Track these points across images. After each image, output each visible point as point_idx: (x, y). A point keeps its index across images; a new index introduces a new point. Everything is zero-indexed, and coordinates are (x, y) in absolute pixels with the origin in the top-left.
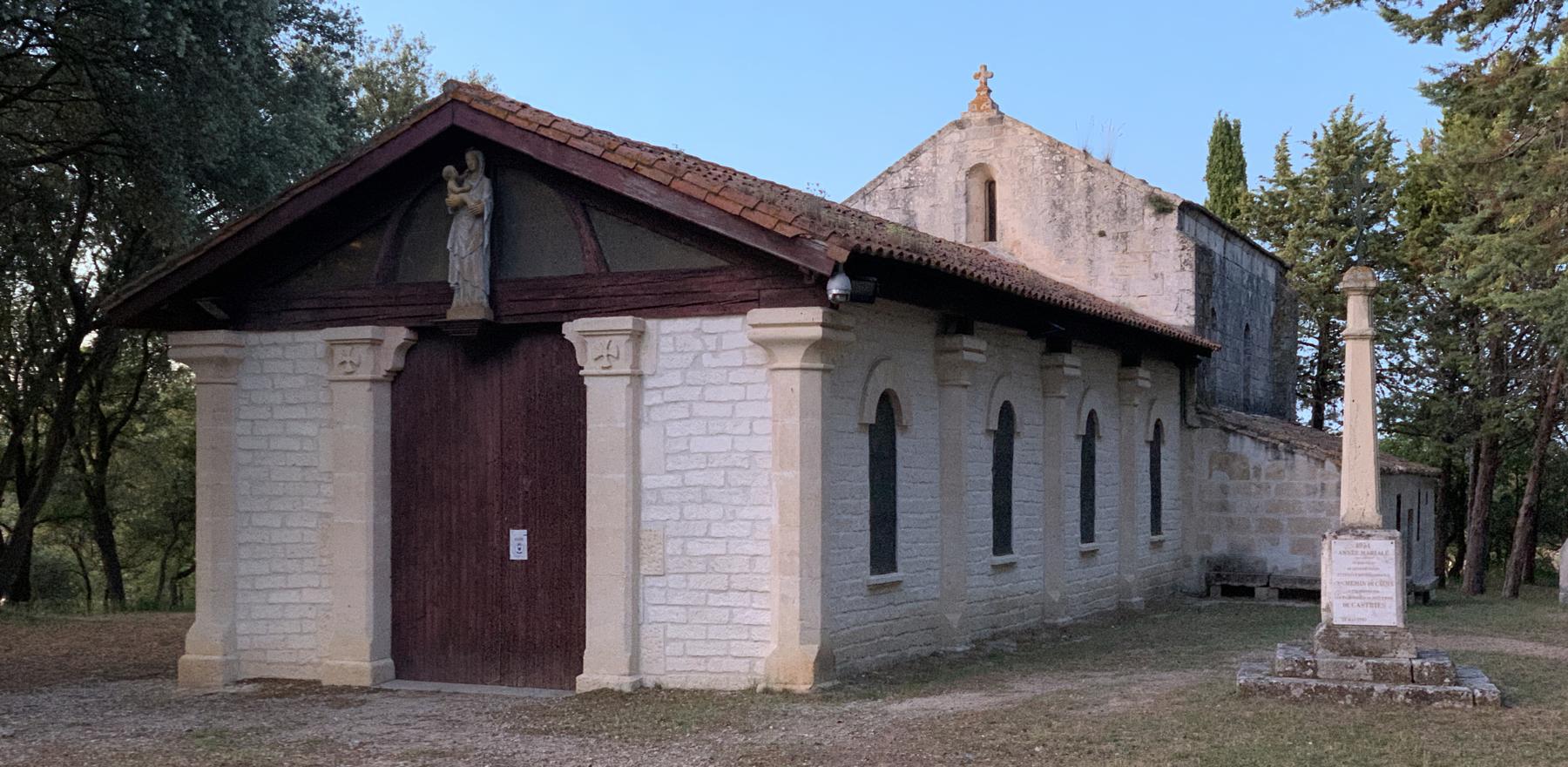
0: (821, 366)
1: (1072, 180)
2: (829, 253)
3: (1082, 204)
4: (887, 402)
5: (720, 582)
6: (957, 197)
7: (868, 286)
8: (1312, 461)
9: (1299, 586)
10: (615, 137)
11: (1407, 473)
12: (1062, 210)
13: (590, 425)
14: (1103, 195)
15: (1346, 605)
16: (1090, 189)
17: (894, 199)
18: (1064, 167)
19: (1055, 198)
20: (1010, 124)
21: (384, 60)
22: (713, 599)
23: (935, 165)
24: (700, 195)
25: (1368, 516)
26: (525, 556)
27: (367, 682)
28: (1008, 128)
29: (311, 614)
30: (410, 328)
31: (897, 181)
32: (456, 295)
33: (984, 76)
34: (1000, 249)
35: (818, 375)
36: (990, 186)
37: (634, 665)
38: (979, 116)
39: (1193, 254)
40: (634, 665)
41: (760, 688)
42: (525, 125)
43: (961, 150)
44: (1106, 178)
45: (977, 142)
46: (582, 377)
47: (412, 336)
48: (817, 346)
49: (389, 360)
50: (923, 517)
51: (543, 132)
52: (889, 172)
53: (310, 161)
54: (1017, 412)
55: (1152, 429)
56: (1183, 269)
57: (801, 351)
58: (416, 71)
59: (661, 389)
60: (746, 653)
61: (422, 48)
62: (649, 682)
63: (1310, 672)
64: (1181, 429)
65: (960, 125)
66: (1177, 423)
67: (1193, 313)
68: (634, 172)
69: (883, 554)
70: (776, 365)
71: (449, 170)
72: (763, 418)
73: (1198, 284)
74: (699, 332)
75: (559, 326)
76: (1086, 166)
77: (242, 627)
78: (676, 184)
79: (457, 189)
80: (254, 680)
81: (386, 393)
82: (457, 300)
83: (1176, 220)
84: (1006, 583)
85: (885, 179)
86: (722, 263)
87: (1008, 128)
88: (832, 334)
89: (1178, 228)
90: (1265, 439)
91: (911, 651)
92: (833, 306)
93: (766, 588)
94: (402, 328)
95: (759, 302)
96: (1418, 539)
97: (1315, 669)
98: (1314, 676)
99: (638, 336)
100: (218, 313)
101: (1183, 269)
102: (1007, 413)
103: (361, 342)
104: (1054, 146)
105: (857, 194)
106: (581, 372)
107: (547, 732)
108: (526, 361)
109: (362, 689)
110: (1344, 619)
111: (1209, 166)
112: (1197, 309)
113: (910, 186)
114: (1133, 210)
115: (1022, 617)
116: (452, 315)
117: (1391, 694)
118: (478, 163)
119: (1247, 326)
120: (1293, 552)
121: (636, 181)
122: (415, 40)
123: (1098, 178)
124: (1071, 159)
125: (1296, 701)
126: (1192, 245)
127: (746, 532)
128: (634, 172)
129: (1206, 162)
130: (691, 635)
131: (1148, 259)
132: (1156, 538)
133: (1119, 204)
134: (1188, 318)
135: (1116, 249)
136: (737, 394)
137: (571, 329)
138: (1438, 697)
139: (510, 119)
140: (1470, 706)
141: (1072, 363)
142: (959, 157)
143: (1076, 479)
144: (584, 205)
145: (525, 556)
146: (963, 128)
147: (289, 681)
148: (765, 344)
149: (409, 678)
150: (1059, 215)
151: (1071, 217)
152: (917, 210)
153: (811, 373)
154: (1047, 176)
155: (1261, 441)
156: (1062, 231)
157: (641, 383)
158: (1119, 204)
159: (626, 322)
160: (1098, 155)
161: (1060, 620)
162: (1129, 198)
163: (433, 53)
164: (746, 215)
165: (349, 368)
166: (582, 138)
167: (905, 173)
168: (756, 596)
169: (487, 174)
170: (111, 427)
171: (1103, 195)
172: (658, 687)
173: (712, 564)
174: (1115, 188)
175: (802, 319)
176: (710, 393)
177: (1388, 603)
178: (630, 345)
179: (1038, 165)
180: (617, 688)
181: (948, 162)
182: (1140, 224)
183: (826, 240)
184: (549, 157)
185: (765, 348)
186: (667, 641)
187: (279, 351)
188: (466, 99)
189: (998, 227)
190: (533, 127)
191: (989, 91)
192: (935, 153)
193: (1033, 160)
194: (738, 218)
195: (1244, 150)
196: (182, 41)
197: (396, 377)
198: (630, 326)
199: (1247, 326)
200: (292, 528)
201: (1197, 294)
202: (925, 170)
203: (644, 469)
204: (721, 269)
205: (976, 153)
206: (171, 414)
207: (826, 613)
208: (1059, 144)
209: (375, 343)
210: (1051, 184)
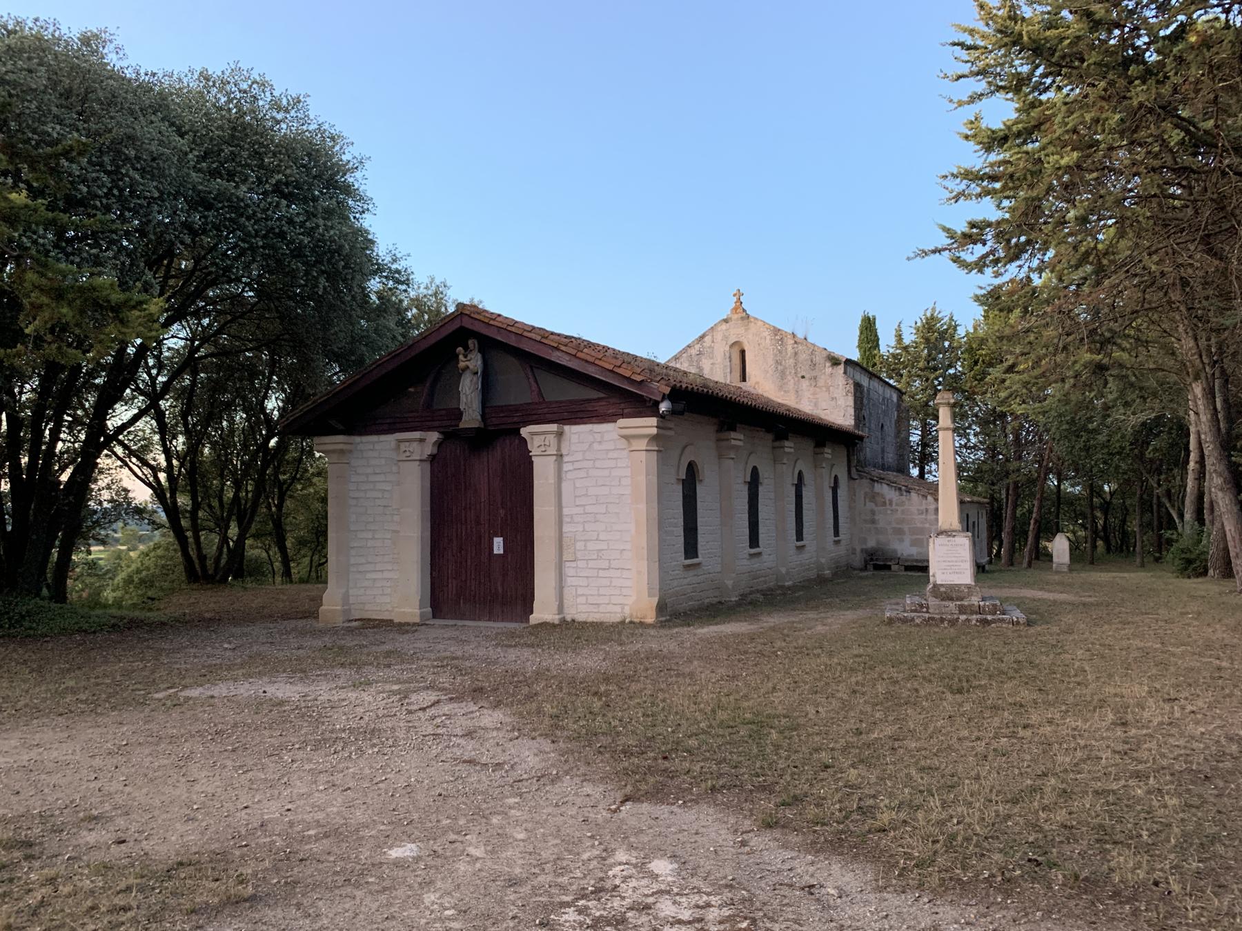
0: (656, 448)
3: (792, 361)
5: (605, 564)
7: (680, 406)
14: (803, 357)
16: (796, 354)
22: (602, 573)
24: (591, 360)
26: (502, 552)
27: (417, 620)
29: (388, 584)
31: (694, 352)
33: (739, 294)
36: (743, 352)
37: (561, 608)
38: (736, 316)
40: (561, 608)
41: (627, 621)
42: (500, 325)
48: (654, 439)
49: (429, 449)
51: (509, 328)
52: (689, 346)
57: (646, 441)
58: (442, 299)
62: (569, 618)
63: (925, 610)
65: (726, 321)
68: (557, 349)
69: (691, 548)
71: (460, 349)
77: (351, 592)
78: (579, 354)
80: (359, 620)
81: (427, 466)
84: (756, 564)
86: (602, 395)
88: (662, 432)
95: (623, 416)
97: (928, 608)
98: (927, 612)
99: (560, 434)
100: (341, 427)
104: (776, 331)
107: (515, 646)
109: (414, 624)
113: (700, 354)
115: (765, 582)
120: (911, 545)
128: (557, 349)
137: (525, 432)
138: (994, 621)
139: (492, 322)
142: (726, 338)
144: (531, 367)
145: (502, 552)
147: (376, 620)
148: (627, 438)
150: (779, 367)
160: (800, 335)
165: (408, 454)
167: (697, 347)
169: (479, 351)
171: (803, 357)
172: (573, 621)
176: (598, 464)
179: (768, 341)
184: (512, 341)
186: (577, 596)
188: (468, 313)
190: (505, 326)
194: (612, 371)
197: (433, 458)
203: (564, 504)
206: (315, 480)
207: (662, 581)
209: (422, 440)
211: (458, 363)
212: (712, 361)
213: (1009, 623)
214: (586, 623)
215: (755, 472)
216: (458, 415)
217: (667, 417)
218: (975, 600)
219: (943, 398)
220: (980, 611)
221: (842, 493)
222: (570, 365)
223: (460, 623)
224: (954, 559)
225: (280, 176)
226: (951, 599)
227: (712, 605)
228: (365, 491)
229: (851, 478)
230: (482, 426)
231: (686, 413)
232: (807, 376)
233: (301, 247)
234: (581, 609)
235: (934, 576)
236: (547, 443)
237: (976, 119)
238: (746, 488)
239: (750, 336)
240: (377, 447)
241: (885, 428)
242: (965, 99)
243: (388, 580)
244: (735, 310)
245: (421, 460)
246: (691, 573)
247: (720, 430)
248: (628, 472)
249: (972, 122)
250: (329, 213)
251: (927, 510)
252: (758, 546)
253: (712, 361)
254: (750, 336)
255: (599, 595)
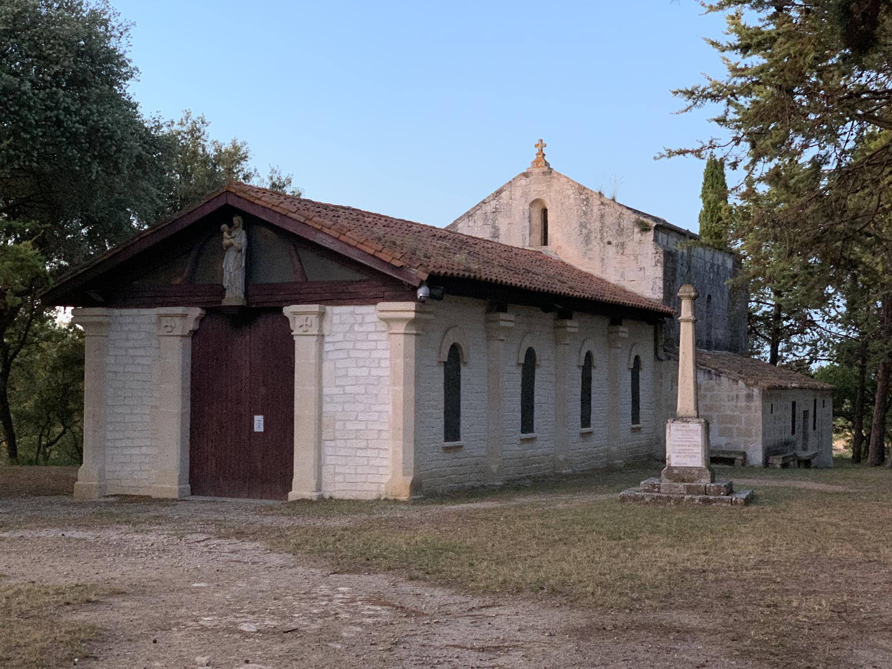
0: (414, 332)
1: (592, 210)
2: (418, 275)
3: (598, 225)
4: (455, 350)
5: (363, 444)
6: (524, 218)
7: (438, 292)
8: (731, 381)
9: (721, 455)
10: (313, 202)
11: (801, 388)
12: (586, 228)
13: (297, 362)
14: (610, 220)
15: (677, 457)
16: (602, 216)
17: (486, 219)
18: (587, 202)
19: (582, 221)
20: (555, 175)
21: (180, 130)
22: (360, 453)
23: (511, 199)
24: (354, 243)
25: (690, 411)
26: (262, 430)
27: (177, 496)
28: (554, 178)
29: (147, 460)
30: (202, 308)
31: (489, 208)
32: (227, 291)
33: (541, 145)
34: (549, 251)
35: (414, 337)
36: (545, 212)
37: (319, 488)
38: (537, 170)
39: (662, 256)
40: (319, 488)
41: (382, 498)
42: (264, 204)
43: (527, 190)
44: (612, 210)
45: (536, 185)
46: (293, 336)
47: (203, 312)
48: (412, 322)
49: (191, 325)
50: (476, 411)
51: (274, 208)
52: (484, 202)
53: (145, 211)
54: (537, 353)
55: (632, 361)
56: (656, 265)
57: (405, 324)
58: (199, 138)
59: (334, 343)
60: (375, 480)
61: (203, 123)
62: (327, 496)
63: (656, 490)
64: (655, 360)
65: (526, 175)
66: (652, 358)
67: (662, 291)
68: (320, 231)
69: (452, 430)
70: (391, 332)
71: (224, 226)
72: (385, 359)
73: (665, 273)
74: (353, 313)
75: (281, 309)
76: (600, 202)
77: (107, 468)
78: (342, 238)
79: (229, 237)
80: (115, 495)
81: (189, 341)
82: (228, 294)
83: (652, 236)
84: (529, 451)
85: (481, 206)
86: (365, 278)
87: (554, 178)
88: (419, 315)
89: (653, 240)
90: (704, 368)
91: (467, 484)
92: (421, 302)
93: (387, 447)
94: (198, 308)
95: (384, 299)
96: (814, 428)
97: (659, 488)
98: (658, 492)
99: (322, 315)
100: (100, 299)
101: (656, 265)
102: (530, 354)
103: (176, 315)
104: (581, 189)
105: (464, 215)
106: (292, 333)
107: (273, 515)
108: (264, 326)
109: (173, 500)
110: (676, 463)
111: (703, 188)
112: (664, 289)
113: (496, 211)
114: (627, 229)
115: (539, 469)
116: (225, 303)
117: (693, 500)
118: (240, 223)
119: (709, 297)
120: (720, 436)
121: (320, 235)
122: (199, 118)
123: (607, 209)
124: (591, 198)
125: (647, 503)
126: (662, 250)
127: (376, 418)
128: (320, 231)
129: (701, 186)
130: (348, 471)
131: (636, 258)
132: (635, 426)
133: (619, 225)
134: (659, 294)
135: (618, 252)
136: (372, 345)
137: (288, 310)
138: (715, 501)
139: (257, 202)
140: (730, 505)
141: (572, 325)
142: (525, 194)
143: (578, 391)
144: (295, 246)
145: (262, 430)
146: (527, 177)
147: (133, 496)
148: (387, 321)
149: (199, 495)
150: (584, 231)
151: (591, 232)
152: (500, 226)
153: (409, 336)
154: (577, 207)
155: (701, 369)
156: (586, 241)
157: (323, 339)
158: (619, 225)
159: (315, 308)
160: (608, 196)
161: (564, 471)
162: (625, 222)
163: (210, 125)
164: (377, 254)
166: (295, 213)
167: (493, 203)
168: (381, 452)
169: (244, 228)
170: (11, 352)
171: (610, 220)
172: (331, 498)
173: (358, 434)
174: (617, 215)
175: (404, 308)
176: (358, 346)
177: (698, 455)
178: (318, 319)
179: (572, 201)
180: (309, 498)
181: (518, 197)
182: (631, 237)
183: (417, 268)
184: (277, 221)
185: (388, 323)
186: (336, 474)
187: (131, 319)
188: (233, 191)
189: (549, 240)
190: (269, 206)
191: (544, 155)
192: (511, 191)
193: (569, 197)
194: (373, 256)
195: (726, 178)
196: (94, 171)
197: (194, 334)
198: (317, 310)
199: (709, 297)
200: (136, 414)
201: (664, 280)
202: (505, 202)
203: (324, 384)
204: (364, 281)
205: (535, 193)
206: (44, 345)
207: (417, 460)
208: (584, 188)
209: (184, 316)
210: (579, 212)
211: (222, 239)
212: (509, 221)
213: (728, 502)
214: (342, 500)
215: (530, 354)
216: (222, 291)
217: (427, 302)
218: (705, 481)
219: (685, 292)
220: (706, 491)
221: (645, 376)
222: (332, 247)
223: (219, 499)
224: (687, 443)
225: (59, 67)
226: (683, 481)
227: (473, 488)
228: (125, 365)
229: (657, 358)
230: (245, 305)
231: (445, 296)
232: (614, 242)
233: (75, 134)
234: (336, 488)
235: (669, 459)
236: (309, 323)
237: (737, 15)
238: (519, 370)
239: (553, 194)
240: (137, 320)
241: (714, 299)
242: (715, 4)
243: (146, 455)
244: (536, 163)
245: (182, 336)
246: (450, 456)
247: (489, 311)
248: (387, 354)
249: (733, 18)
250: (100, 99)
251: (737, 396)
252: (532, 431)
253: (509, 221)
254: (553, 194)
255: (356, 474)
